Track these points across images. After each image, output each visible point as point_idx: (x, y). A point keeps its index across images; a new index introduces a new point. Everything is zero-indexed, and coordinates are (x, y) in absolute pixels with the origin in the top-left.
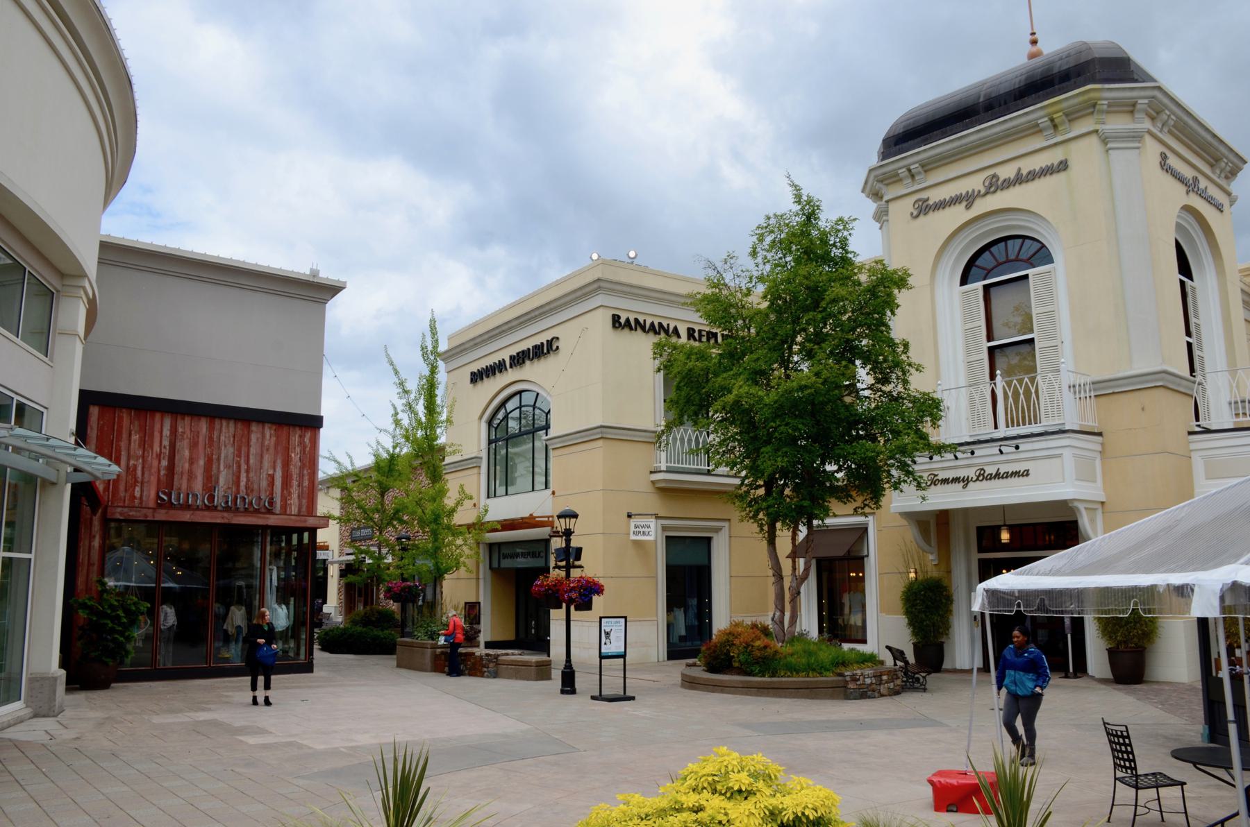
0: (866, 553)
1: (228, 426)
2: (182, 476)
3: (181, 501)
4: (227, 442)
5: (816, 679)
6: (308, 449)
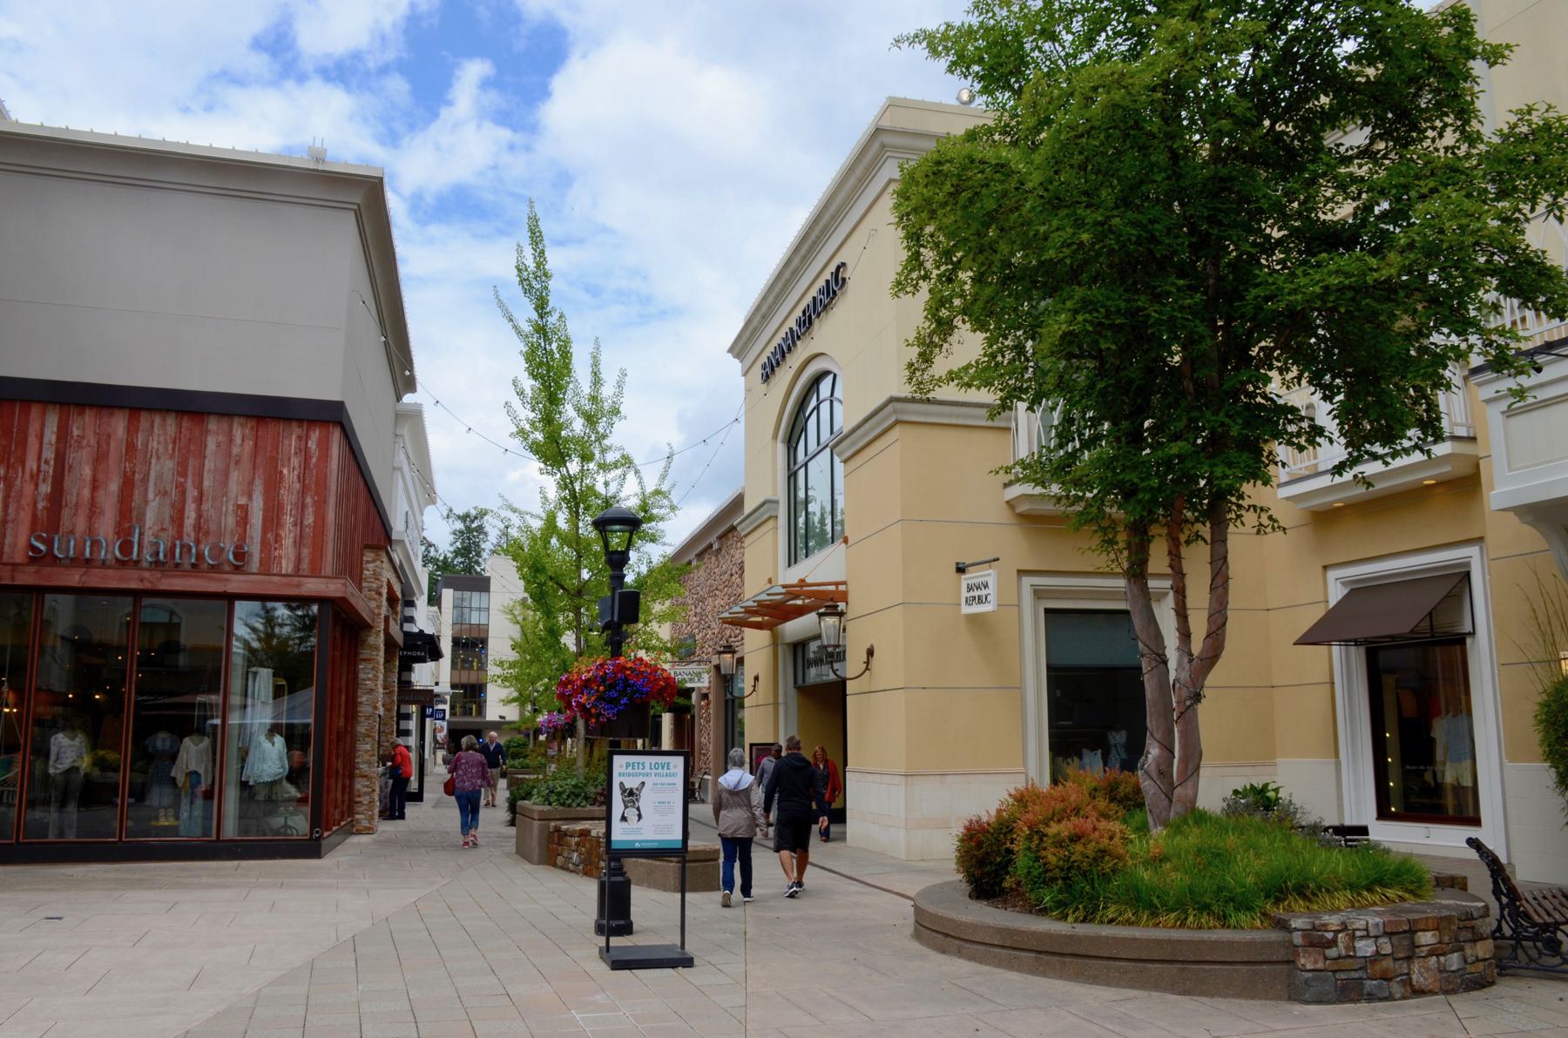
0: (1468, 628)
1: (163, 425)
2: (77, 510)
3: (72, 552)
4: (161, 450)
5: (1205, 935)
6: (314, 460)
